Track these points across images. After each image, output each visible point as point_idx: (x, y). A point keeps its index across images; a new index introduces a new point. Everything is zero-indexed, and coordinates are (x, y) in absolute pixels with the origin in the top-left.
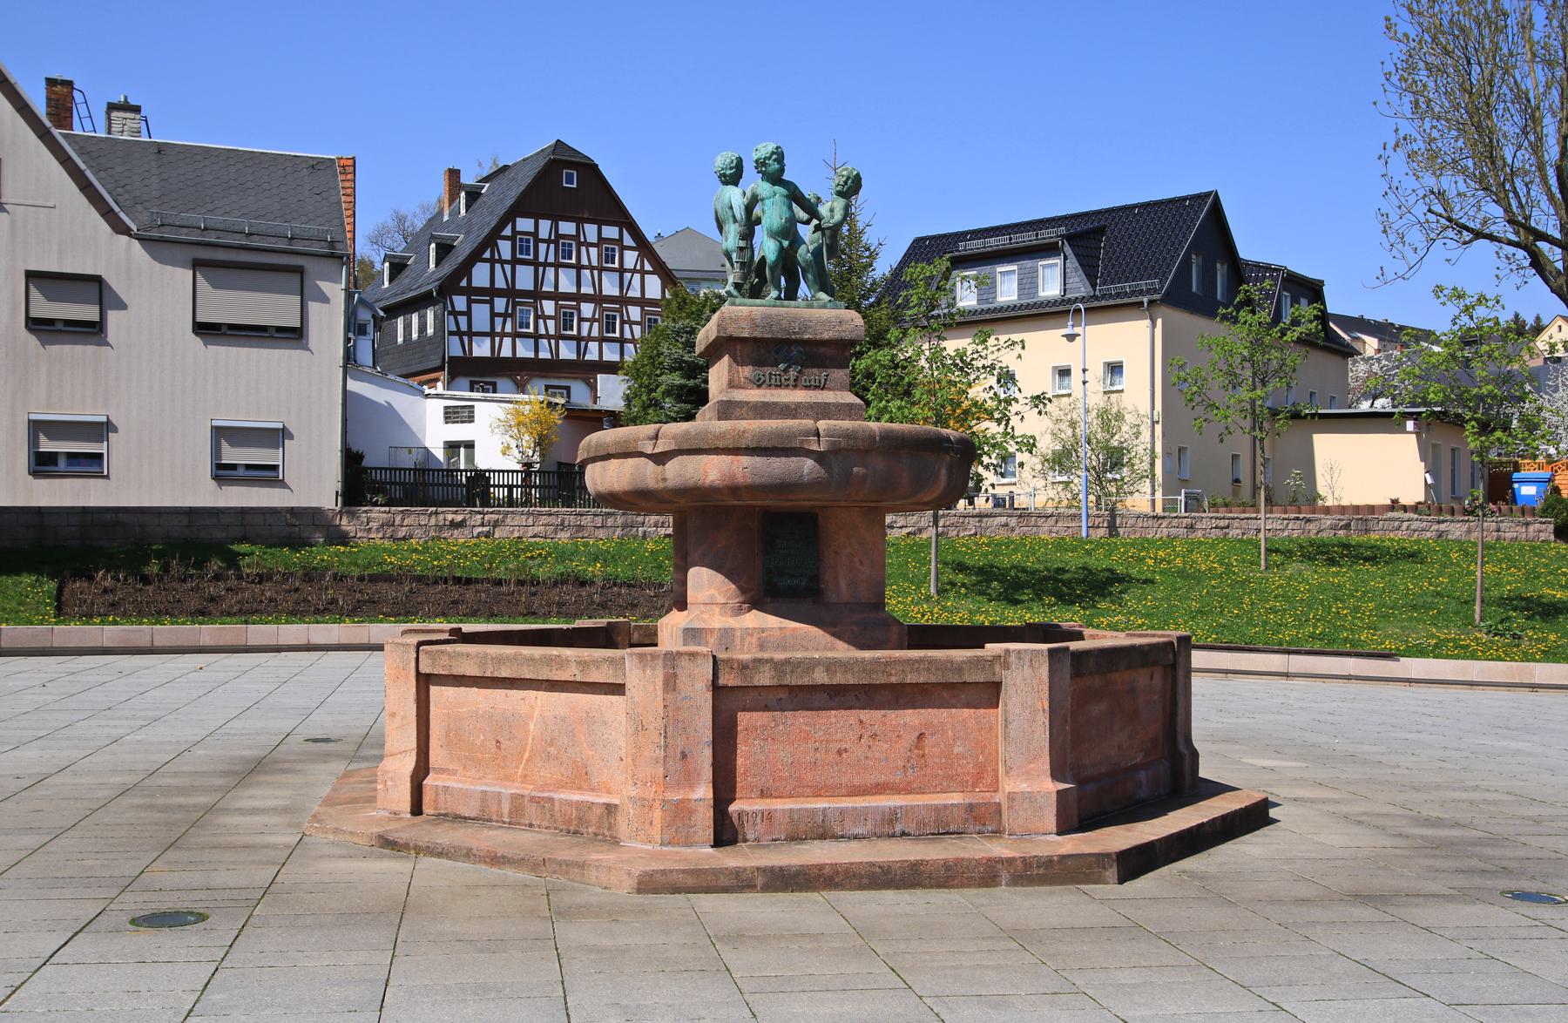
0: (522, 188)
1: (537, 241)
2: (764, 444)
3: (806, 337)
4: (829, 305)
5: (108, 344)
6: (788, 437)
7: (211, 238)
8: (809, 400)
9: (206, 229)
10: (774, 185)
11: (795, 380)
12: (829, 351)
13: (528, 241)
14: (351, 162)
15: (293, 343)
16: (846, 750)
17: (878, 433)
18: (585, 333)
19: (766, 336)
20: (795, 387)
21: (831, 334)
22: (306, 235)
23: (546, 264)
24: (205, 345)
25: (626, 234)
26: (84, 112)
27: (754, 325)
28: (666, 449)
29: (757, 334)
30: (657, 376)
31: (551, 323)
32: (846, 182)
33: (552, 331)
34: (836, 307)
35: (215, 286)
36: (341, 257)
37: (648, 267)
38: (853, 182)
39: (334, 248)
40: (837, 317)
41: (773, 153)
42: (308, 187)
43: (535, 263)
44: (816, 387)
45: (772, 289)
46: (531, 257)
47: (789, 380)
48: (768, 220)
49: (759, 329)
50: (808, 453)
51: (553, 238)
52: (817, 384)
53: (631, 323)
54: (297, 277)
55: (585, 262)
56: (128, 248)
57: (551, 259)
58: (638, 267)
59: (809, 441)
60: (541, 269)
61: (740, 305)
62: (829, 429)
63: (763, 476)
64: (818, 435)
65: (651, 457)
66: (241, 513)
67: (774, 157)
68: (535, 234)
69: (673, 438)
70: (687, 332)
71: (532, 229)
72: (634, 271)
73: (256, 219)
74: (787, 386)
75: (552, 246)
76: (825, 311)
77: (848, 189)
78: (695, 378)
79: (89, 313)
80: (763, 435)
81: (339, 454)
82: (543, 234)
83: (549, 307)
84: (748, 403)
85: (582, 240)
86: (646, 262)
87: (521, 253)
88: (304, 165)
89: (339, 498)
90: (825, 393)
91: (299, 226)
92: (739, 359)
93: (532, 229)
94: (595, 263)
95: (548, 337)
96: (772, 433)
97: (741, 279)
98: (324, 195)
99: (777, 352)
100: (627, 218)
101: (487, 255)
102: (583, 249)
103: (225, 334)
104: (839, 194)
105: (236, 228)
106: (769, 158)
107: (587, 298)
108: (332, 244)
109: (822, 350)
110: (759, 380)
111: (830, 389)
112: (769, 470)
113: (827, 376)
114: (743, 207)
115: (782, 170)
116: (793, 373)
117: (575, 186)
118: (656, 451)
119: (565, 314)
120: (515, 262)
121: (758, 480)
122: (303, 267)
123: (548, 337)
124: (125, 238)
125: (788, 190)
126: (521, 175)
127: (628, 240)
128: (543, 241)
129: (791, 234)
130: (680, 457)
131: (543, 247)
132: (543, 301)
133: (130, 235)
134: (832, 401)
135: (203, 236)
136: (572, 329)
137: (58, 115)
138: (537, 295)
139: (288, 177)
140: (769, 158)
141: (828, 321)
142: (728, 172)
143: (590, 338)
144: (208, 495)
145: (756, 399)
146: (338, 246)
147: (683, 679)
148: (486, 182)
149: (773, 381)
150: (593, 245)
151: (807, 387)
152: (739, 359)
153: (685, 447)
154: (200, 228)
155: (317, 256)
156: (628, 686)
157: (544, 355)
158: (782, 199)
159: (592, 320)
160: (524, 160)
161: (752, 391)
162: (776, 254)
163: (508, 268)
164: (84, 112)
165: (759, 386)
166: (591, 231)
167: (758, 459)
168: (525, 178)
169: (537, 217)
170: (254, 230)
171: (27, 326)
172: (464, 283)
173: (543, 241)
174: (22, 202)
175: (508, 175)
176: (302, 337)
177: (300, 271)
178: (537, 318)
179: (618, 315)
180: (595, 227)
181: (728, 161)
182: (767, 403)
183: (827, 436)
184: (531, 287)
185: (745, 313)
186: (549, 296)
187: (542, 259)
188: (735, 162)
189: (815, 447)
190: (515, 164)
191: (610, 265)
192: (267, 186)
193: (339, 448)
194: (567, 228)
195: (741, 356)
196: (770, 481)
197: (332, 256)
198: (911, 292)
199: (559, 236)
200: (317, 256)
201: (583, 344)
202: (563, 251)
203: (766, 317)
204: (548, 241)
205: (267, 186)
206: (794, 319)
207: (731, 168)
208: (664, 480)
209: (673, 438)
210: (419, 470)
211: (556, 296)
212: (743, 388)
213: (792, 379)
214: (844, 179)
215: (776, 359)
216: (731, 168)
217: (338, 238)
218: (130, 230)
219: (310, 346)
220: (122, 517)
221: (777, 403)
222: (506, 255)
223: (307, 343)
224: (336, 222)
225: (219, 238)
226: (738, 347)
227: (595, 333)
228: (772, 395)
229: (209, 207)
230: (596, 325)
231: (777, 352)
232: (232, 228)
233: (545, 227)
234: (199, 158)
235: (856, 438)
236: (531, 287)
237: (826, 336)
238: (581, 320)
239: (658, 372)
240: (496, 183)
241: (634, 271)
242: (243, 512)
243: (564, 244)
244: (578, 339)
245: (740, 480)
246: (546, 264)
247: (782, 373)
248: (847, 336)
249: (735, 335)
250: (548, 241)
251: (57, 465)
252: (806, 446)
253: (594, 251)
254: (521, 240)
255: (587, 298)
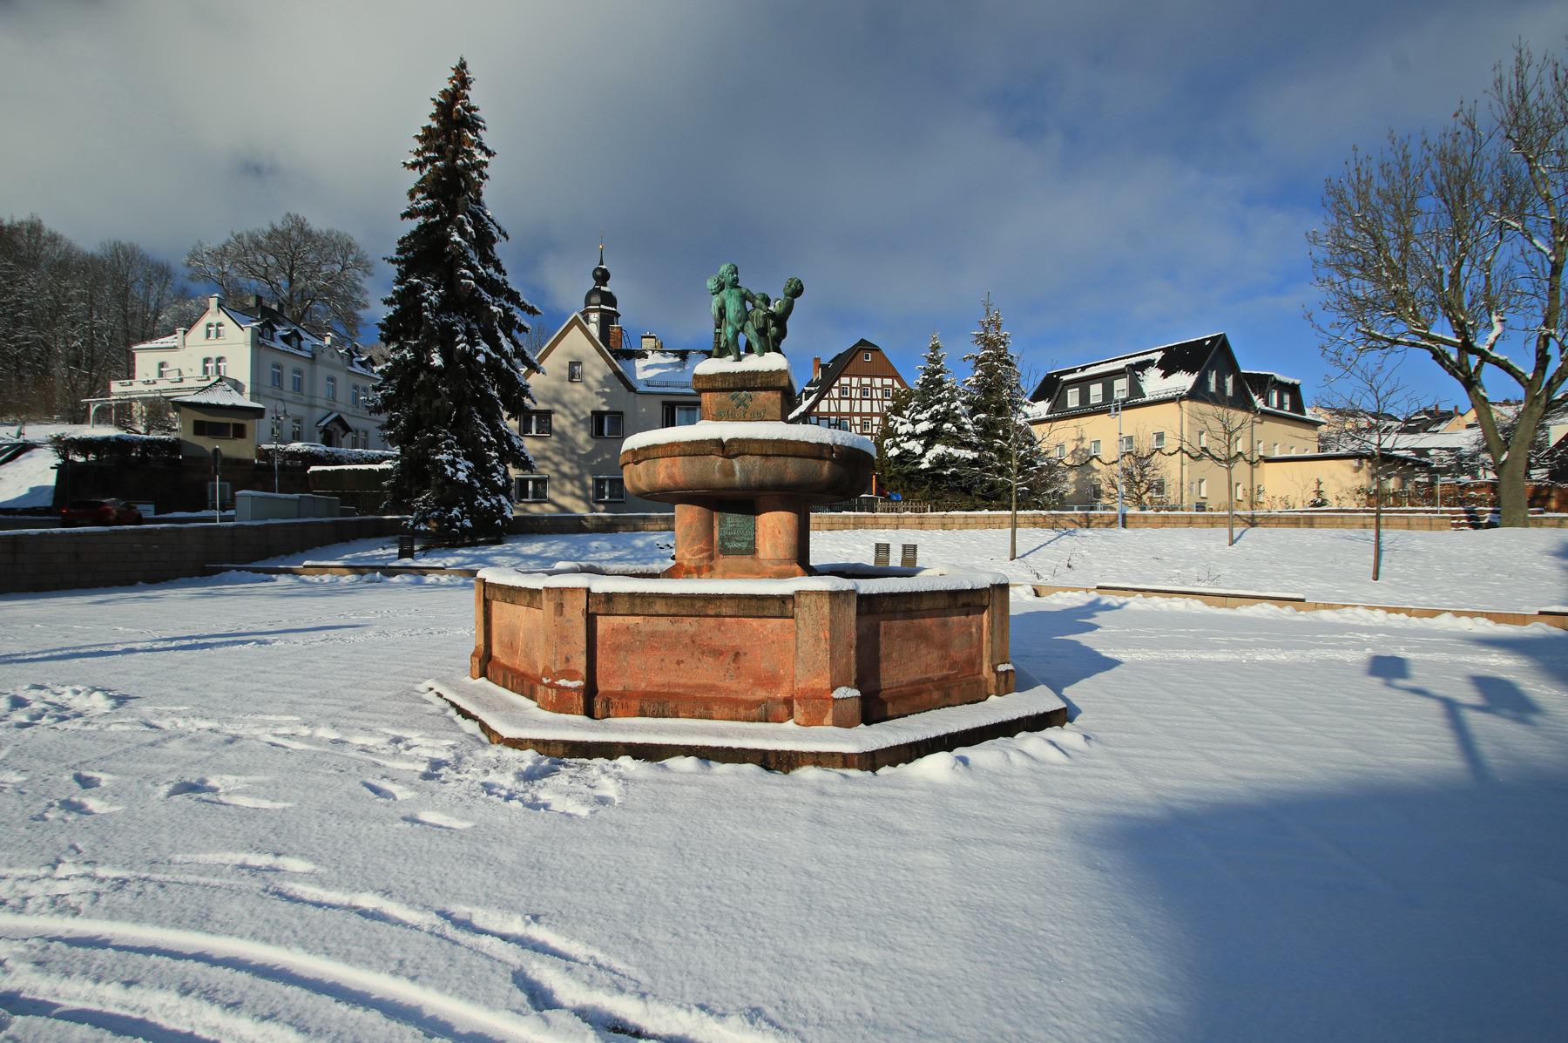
16: (682, 662)
26: (627, 340)
31: (858, 428)
43: (872, 399)
45: (1470, 356)
53: (855, 425)
55: (874, 397)
57: (858, 396)
68: (850, 385)
82: (854, 385)
101: (827, 396)
120: (840, 399)
131: (854, 391)
138: (851, 414)
147: (567, 609)
156: (325, 379)
163: (837, 402)
164: (627, 340)
166: (878, 382)
172: (815, 410)
186: (857, 414)
194: (866, 381)
204: (857, 388)
210: (866, 673)
211: (860, 414)
222: (836, 396)
233: (855, 381)
250: (857, 388)
253: (879, 392)
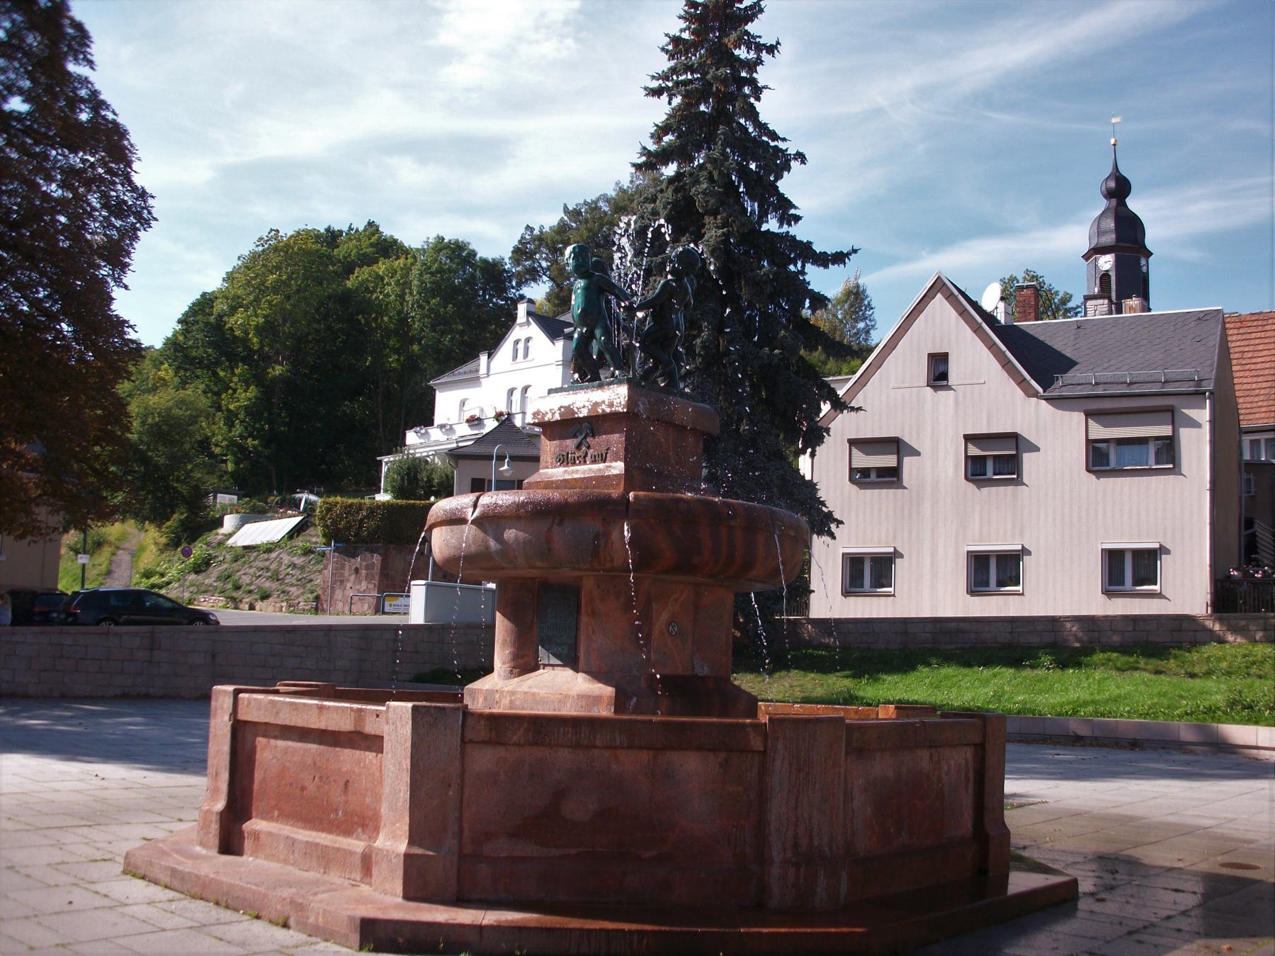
5: (905, 488)
7: (1136, 390)
9: (1097, 384)
54: (1170, 414)
56: (1037, 405)
66: (255, 631)
79: (889, 461)
81: (1208, 568)
89: (1209, 608)
105: (1121, 380)
122: (1172, 406)
124: (1034, 400)
133: (1037, 397)
135: (1093, 390)
137: (1025, 312)
144: (1096, 604)
155: (1117, 397)
171: (852, 480)
174: (963, 382)
193: (1208, 563)
198: (380, 384)
200: (1117, 397)
218: (1038, 392)
220: (962, 625)
223: (1180, 470)
225: (1105, 390)
229: (1106, 365)
242: (1135, 619)
251: (1123, 584)
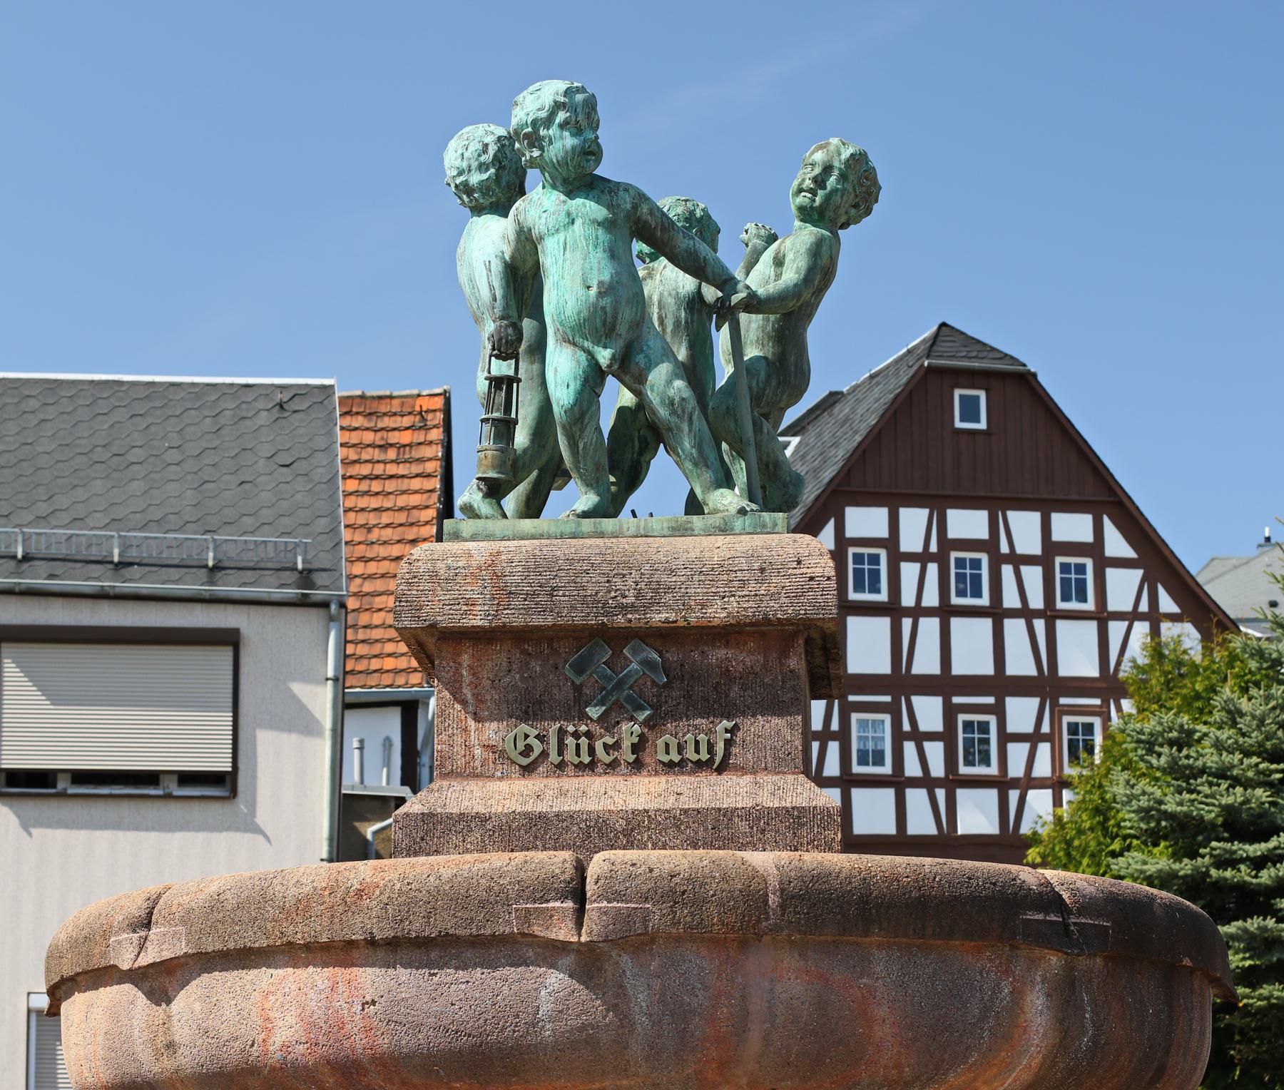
0: (858, 438)
1: (897, 558)
2: (416, 927)
3: (659, 617)
4: (738, 524)
6: (482, 904)
8: (670, 803)
10: (570, 194)
11: (636, 748)
12: (740, 658)
13: (875, 559)
14: (439, 403)
15: (215, 810)
17: (773, 883)
18: (1016, 769)
19: (537, 621)
20: (637, 766)
21: (733, 605)
22: (250, 558)
23: (918, 612)
24: (26, 827)
25: (1109, 528)
27: (503, 593)
28: (167, 955)
29: (514, 617)
30: (1114, 854)
31: (935, 752)
32: (820, 182)
33: (938, 769)
34: (762, 529)
35: (57, 697)
36: (324, 605)
37: (1167, 604)
38: (843, 177)
39: (311, 585)
40: (751, 557)
41: (557, 106)
42: (266, 450)
44: (700, 765)
46: (883, 596)
47: (617, 746)
48: (554, 294)
49: (516, 602)
50: (551, 952)
51: (933, 548)
52: (704, 756)
54: (226, 654)
55: (1011, 599)
57: (931, 598)
58: (1144, 607)
59: (549, 914)
60: (907, 623)
61: (474, 538)
62: (611, 876)
63: (418, 1027)
64: (579, 896)
65: (138, 977)
67: (561, 116)
68: (891, 542)
69: (183, 922)
70: (1171, 743)
71: (883, 532)
72: (1132, 616)
73: (143, 528)
74: (613, 766)
75: (933, 569)
76: (721, 541)
77: (828, 198)
78: (1193, 855)
80: (409, 899)
82: (911, 539)
83: (929, 712)
84: (483, 819)
85: (1004, 549)
86: (1162, 593)
87: (859, 587)
88: (261, 404)
90: (728, 780)
91: (233, 542)
92: (467, 693)
93: (883, 532)
94: (1036, 602)
95: (927, 782)
96: (436, 893)
97: (494, 467)
98: (301, 466)
99: (579, 668)
100: (1116, 495)
102: (1007, 571)
103: (63, 795)
104: (806, 214)
105: (95, 553)
106: (548, 121)
107: (1022, 687)
108: (306, 578)
109: (718, 654)
110: (528, 750)
111: (742, 770)
112: (435, 1007)
113: (733, 731)
114: (497, 267)
115: (591, 152)
116: (629, 731)
117: (983, 425)
118: (144, 960)
119: (1073, 729)
121: (408, 1042)
123: (927, 782)
125: (609, 207)
126: (860, 411)
127: (1116, 544)
128: (911, 557)
129: (622, 329)
130: (205, 978)
131: (909, 572)
132: (916, 700)
134: (744, 802)
136: (986, 761)
139: (224, 432)
140: (548, 121)
141: (724, 568)
142: (475, 178)
143: (1029, 782)
145: (514, 806)
146: (319, 578)
148: (794, 435)
149: (570, 755)
150: (1030, 560)
151: (670, 767)
152: (467, 693)
153: (211, 946)
154: (14, 557)
157: (921, 822)
158: (591, 231)
159: (1034, 739)
160: (872, 377)
161: (504, 786)
162: (575, 386)
165: (527, 770)
167: (403, 973)
168: (867, 416)
169: (893, 500)
170: (133, 554)
173: (911, 557)
175: (841, 411)
176: (234, 793)
177: (230, 639)
178: (899, 737)
179: (1097, 722)
180: (1035, 518)
181: (475, 147)
182: (542, 817)
183: (601, 897)
184: (884, 667)
185: (478, 560)
186: (927, 685)
187: (908, 600)
188: (492, 149)
189: (563, 932)
190: (855, 389)
191: (1074, 605)
192: (173, 456)
195: (475, 686)
196: (441, 1042)
197: (303, 603)
199: (947, 545)
201: (1014, 795)
202: (960, 578)
203: (535, 566)
204: (922, 558)
205: (173, 456)
206: (623, 567)
207: (482, 167)
208: (171, 1046)
209: (183, 922)
212: (477, 776)
213: (626, 744)
214: (817, 171)
215: (578, 689)
216: (482, 167)
217: (324, 561)
219: (262, 818)
221: (572, 815)
224: (322, 524)
225: (51, 576)
226: (466, 659)
227: (1043, 768)
228: (563, 793)
229: (42, 509)
230: (1044, 749)
231: (579, 668)
232: (84, 554)
233: (914, 522)
234: (34, 403)
235: (699, 902)
236: (884, 667)
237: (718, 613)
238: (1006, 738)
239: (1116, 846)
240: (812, 432)
241: (1132, 616)
243: (960, 563)
244: (1002, 784)
245: (359, 1043)
246: (918, 612)
247: (596, 729)
248: (781, 608)
249: (444, 621)
250: (922, 558)
252: (537, 930)
253: (1033, 575)
254: (858, 558)
255: (1022, 687)
